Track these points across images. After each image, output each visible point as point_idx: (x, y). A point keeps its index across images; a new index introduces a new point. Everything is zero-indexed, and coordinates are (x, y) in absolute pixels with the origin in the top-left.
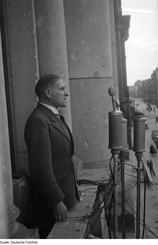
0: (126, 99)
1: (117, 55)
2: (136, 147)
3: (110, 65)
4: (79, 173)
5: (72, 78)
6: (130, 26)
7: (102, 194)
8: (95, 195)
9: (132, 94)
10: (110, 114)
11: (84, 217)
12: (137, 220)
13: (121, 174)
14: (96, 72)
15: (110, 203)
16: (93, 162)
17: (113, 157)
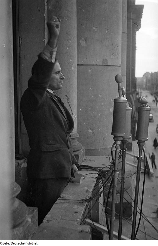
0: (133, 90)
1: (127, 45)
2: (138, 135)
3: (119, 54)
4: (81, 158)
5: (80, 64)
6: (143, 16)
7: (102, 180)
8: (95, 180)
9: (139, 85)
10: (115, 101)
11: (83, 200)
12: (134, 207)
13: (122, 161)
14: (104, 59)
15: (109, 189)
16: (95, 149)
17: (115, 143)
